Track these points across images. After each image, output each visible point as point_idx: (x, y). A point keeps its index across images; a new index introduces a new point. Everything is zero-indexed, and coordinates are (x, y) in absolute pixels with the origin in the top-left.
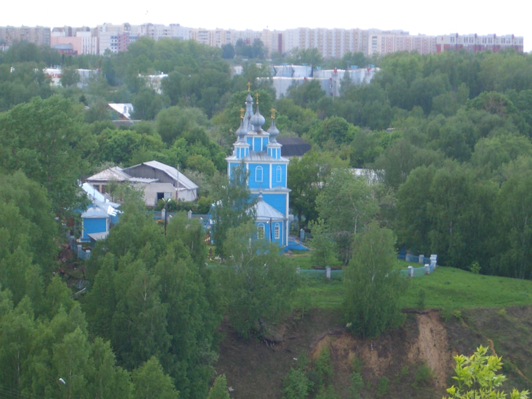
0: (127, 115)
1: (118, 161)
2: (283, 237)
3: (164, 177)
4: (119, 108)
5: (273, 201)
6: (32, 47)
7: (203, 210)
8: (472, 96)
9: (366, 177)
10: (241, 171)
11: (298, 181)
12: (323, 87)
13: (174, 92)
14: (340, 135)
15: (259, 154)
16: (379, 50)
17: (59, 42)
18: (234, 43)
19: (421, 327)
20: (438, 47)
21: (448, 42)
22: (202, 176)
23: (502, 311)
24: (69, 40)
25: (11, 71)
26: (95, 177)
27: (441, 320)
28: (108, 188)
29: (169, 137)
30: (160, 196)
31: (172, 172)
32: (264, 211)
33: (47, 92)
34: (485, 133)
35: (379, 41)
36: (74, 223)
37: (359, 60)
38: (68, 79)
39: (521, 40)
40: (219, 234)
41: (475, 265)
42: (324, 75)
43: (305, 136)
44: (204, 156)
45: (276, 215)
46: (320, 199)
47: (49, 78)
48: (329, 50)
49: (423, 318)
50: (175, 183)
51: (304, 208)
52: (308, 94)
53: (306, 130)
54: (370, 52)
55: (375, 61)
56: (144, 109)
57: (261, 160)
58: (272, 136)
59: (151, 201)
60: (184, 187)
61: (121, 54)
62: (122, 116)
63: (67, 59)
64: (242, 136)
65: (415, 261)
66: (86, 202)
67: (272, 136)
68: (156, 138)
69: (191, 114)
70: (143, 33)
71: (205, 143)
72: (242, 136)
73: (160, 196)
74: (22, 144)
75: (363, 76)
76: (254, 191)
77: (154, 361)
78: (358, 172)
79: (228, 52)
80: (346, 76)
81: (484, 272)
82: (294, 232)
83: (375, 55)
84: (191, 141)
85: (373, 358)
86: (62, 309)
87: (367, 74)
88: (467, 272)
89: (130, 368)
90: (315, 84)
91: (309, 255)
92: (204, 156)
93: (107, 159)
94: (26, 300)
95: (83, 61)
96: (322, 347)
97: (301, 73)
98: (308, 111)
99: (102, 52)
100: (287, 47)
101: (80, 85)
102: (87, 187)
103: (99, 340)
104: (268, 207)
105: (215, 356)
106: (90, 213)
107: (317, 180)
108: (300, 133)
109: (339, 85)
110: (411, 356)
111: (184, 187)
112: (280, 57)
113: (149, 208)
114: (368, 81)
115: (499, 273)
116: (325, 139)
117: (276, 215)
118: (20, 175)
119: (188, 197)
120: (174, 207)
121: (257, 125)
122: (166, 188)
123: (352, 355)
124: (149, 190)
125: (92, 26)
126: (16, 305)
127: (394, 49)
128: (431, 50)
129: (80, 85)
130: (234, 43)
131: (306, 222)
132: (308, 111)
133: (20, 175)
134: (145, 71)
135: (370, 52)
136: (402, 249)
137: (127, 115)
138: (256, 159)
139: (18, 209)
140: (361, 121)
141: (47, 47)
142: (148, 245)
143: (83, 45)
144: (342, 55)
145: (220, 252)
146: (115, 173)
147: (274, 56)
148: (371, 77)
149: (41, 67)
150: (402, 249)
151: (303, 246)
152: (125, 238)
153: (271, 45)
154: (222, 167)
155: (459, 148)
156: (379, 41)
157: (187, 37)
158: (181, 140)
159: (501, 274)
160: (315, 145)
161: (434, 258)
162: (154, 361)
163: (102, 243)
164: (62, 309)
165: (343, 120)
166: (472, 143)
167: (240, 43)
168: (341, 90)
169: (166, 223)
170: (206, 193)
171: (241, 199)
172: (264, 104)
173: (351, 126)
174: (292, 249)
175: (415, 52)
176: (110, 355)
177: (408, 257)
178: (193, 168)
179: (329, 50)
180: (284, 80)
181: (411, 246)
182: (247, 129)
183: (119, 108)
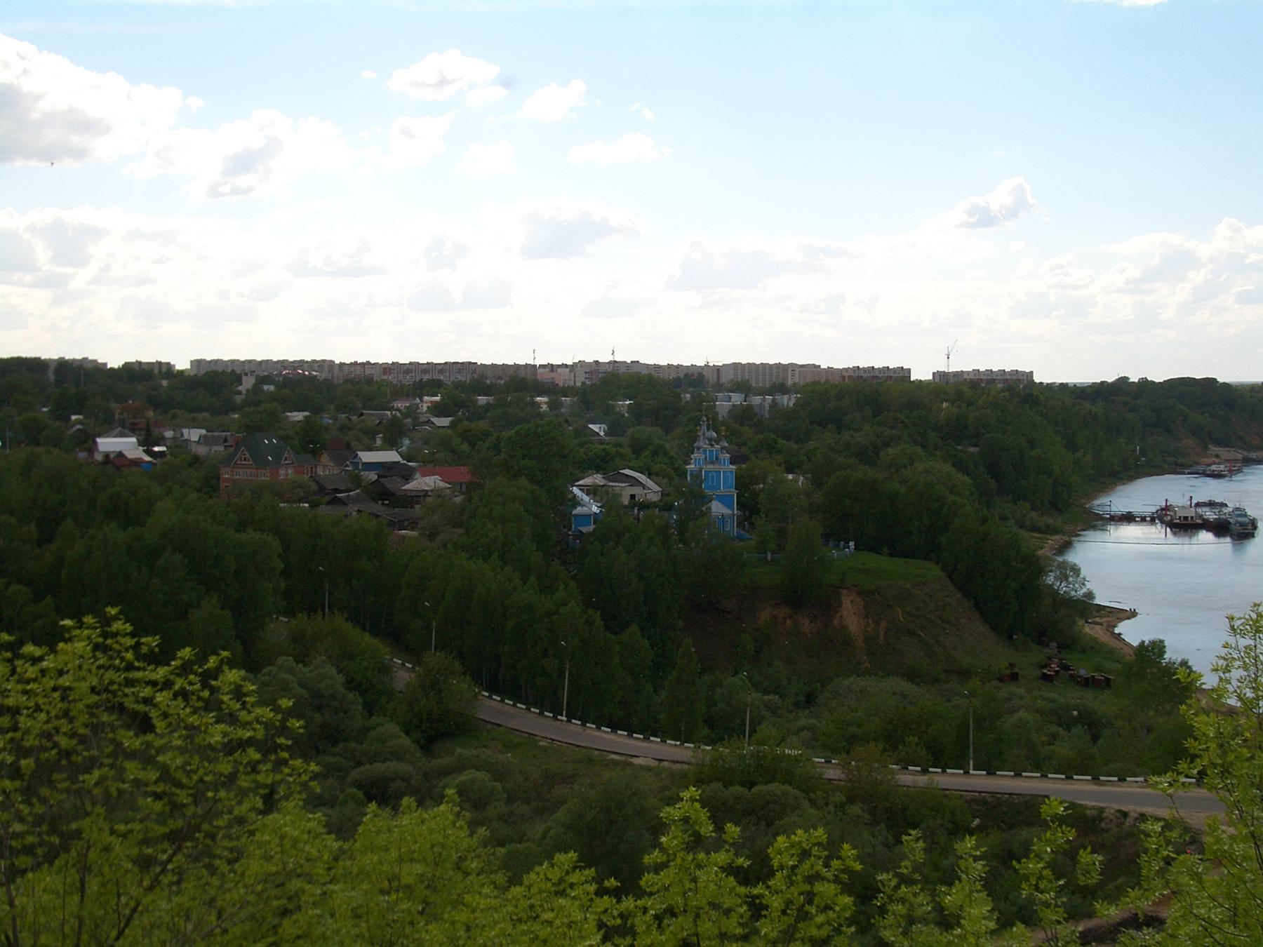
0: (602, 434)
1: (598, 469)
2: (732, 529)
3: (636, 482)
4: (595, 427)
5: (724, 500)
6: (524, 380)
7: (668, 508)
8: (874, 416)
9: (796, 480)
10: (697, 476)
11: (742, 484)
12: (756, 410)
13: (638, 413)
14: (771, 448)
15: (713, 463)
16: (797, 380)
17: (544, 376)
18: (682, 375)
19: (843, 599)
20: (843, 377)
21: (851, 374)
22: (665, 480)
23: (908, 586)
24: (552, 375)
25: (108, 609)
26: (581, 482)
27: (859, 593)
28: (592, 491)
29: (637, 450)
30: (633, 497)
31: (642, 478)
32: (717, 508)
33: (541, 416)
34: (886, 445)
35: (797, 373)
36: (566, 519)
37: (781, 388)
38: (554, 406)
39: (909, 370)
40: (682, 526)
41: (885, 550)
42: (757, 400)
43: (744, 449)
44: (668, 467)
45: (727, 511)
46: (761, 497)
47: (539, 405)
48: (757, 381)
49: (845, 592)
50: (644, 486)
51: (748, 507)
52: (744, 415)
53: (745, 444)
54: (790, 382)
55: (795, 389)
56: (615, 428)
57: (714, 467)
58: (722, 448)
59: (626, 501)
60: (651, 489)
61: (593, 385)
62: (598, 434)
63: (551, 389)
64: (699, 448)
65: (837, 547)
66: (576, 502)
67: (722, 448)
68: (627, 451)
69: (649, 431)
70: (610, 369)
71: (666, 454)
72: (699, 448)
73: (633, 497)
74: (524, 457)
75: (788, 401)
76: (708, 492)
77: (634, 628)
78: (790, 477)
79: (677, 382)
80: (774, 400)
81: (891, 555)
82: (740, 524)
83: (794, 384)
84: (655, 453)
85: (806, 625)
86: (562, 587)
87: (789, 399)
88: (1221, 480)
89: (616, 633)
90: (750, 407)
91: (753, 542)
92: (668, 467)
93: (589, 468)
94: (533, 579)
95: (566, 391)
96: (765, 615)
97: (737, 399)
98: (746, 428)
99: (579, 384)
100: (724, 379)
101: (563, 410)
102: (575, 490)
103: (591, 611)
104: (720, 505)
105: (681, 623)
106: (579, 510)
107: (757, 483)
108: (740, 447)
109: (767, 408)
110: (836, 622)
111: (651, 489)
112: (719, 387)
113: (626, 507)
114: (791, 405)
115: (903, 555)
116: (760, 451)
117: (727, 511)
118: (523, 481)
119: (655, 498)
120: (645, 506)
121: (710, 440)
122: (636, 490)
123: (788, 622)
124: (625, 493)
125: (570, 363)
126: (525, 583)
127: (809, 380)
128: (837, 380)
129: (563, 410)
130: (682, 375)
131: (750, 517)
132: (746, 428)
133: (523, 481)
134: (614, 398)
135: (790, 382)
136: (826, 537)
137: (602, 434)
138: (710, 466)
139: (522, 508)
140: (787, 437)
141: (536, 381)
142: (627, 536)
143: (563, 379)
144: (768, 386)
145: (682, 540)
146: (597, 479)
147: (713, 386)
148: (793, 401)
149: (532, 397)
150: (826, 537)
151: (747, 536)
152: (611, 528)
153: (711, 378)
154: (683, 474)
155: (868, 455)
156: (797, 373)
157: (645, 372)
158: (647, 453)
159: (906, 557)
160: (752, 456)
161: (852, 544)
162: (634, 628)
163: (590, 534)
164: (562, 587)
165: (773, 436)
166: (877, 453)
167: (686, 375)
168: (770, 412)
169: (638, 519)
170: (668, 495)
171: (697, 499)
172: (714, 424)
173: (780, 441)
174: (740, 539)
175: (827, 381)
176: (599, 622)
177: (831, 544)
178: (657, 475)
179: (757, 381)
180: (725, 404)
181: (836, 535)
182: (701, 443)
183: (595, 427)
